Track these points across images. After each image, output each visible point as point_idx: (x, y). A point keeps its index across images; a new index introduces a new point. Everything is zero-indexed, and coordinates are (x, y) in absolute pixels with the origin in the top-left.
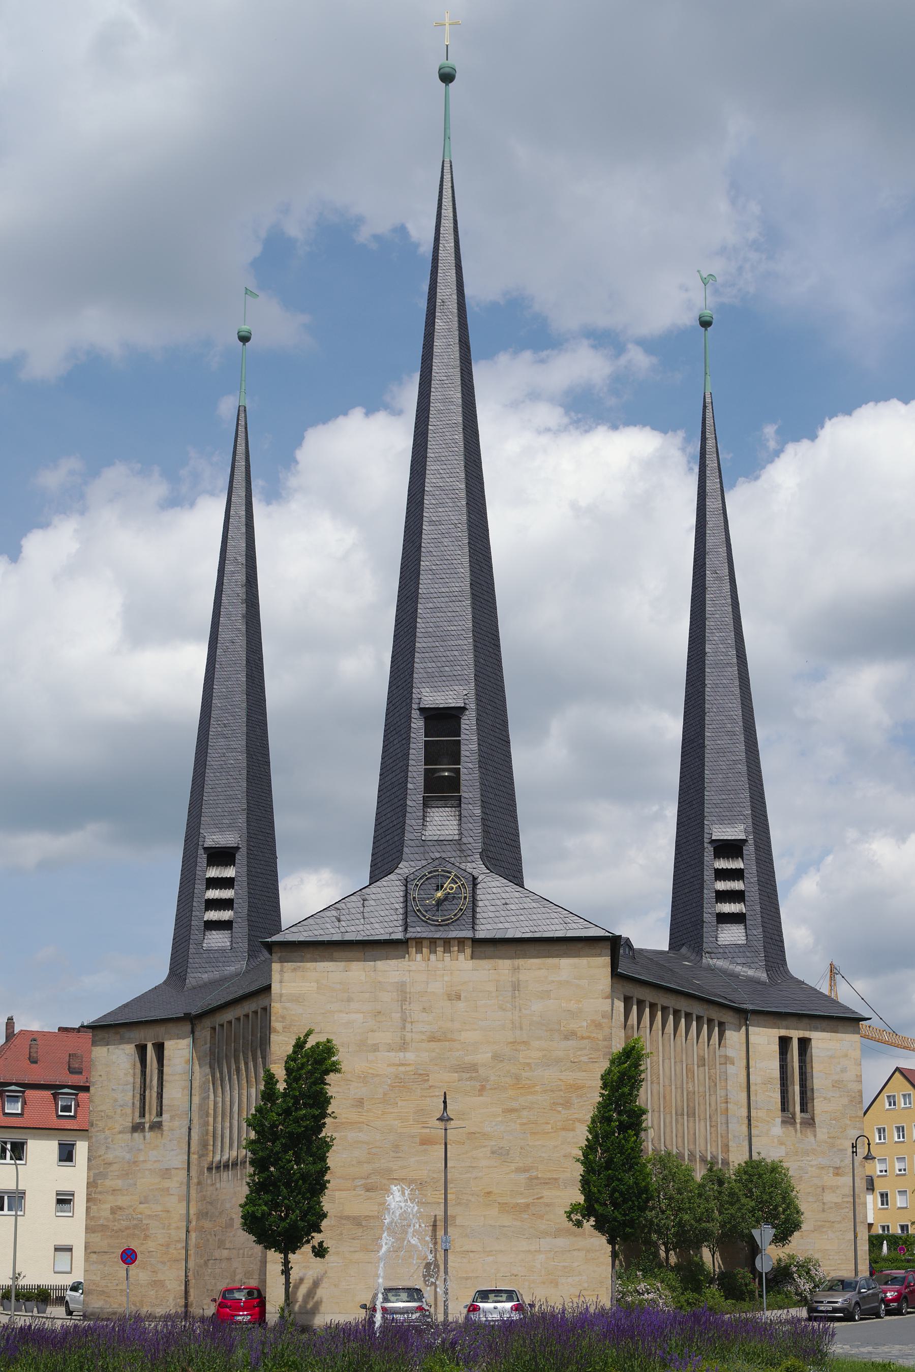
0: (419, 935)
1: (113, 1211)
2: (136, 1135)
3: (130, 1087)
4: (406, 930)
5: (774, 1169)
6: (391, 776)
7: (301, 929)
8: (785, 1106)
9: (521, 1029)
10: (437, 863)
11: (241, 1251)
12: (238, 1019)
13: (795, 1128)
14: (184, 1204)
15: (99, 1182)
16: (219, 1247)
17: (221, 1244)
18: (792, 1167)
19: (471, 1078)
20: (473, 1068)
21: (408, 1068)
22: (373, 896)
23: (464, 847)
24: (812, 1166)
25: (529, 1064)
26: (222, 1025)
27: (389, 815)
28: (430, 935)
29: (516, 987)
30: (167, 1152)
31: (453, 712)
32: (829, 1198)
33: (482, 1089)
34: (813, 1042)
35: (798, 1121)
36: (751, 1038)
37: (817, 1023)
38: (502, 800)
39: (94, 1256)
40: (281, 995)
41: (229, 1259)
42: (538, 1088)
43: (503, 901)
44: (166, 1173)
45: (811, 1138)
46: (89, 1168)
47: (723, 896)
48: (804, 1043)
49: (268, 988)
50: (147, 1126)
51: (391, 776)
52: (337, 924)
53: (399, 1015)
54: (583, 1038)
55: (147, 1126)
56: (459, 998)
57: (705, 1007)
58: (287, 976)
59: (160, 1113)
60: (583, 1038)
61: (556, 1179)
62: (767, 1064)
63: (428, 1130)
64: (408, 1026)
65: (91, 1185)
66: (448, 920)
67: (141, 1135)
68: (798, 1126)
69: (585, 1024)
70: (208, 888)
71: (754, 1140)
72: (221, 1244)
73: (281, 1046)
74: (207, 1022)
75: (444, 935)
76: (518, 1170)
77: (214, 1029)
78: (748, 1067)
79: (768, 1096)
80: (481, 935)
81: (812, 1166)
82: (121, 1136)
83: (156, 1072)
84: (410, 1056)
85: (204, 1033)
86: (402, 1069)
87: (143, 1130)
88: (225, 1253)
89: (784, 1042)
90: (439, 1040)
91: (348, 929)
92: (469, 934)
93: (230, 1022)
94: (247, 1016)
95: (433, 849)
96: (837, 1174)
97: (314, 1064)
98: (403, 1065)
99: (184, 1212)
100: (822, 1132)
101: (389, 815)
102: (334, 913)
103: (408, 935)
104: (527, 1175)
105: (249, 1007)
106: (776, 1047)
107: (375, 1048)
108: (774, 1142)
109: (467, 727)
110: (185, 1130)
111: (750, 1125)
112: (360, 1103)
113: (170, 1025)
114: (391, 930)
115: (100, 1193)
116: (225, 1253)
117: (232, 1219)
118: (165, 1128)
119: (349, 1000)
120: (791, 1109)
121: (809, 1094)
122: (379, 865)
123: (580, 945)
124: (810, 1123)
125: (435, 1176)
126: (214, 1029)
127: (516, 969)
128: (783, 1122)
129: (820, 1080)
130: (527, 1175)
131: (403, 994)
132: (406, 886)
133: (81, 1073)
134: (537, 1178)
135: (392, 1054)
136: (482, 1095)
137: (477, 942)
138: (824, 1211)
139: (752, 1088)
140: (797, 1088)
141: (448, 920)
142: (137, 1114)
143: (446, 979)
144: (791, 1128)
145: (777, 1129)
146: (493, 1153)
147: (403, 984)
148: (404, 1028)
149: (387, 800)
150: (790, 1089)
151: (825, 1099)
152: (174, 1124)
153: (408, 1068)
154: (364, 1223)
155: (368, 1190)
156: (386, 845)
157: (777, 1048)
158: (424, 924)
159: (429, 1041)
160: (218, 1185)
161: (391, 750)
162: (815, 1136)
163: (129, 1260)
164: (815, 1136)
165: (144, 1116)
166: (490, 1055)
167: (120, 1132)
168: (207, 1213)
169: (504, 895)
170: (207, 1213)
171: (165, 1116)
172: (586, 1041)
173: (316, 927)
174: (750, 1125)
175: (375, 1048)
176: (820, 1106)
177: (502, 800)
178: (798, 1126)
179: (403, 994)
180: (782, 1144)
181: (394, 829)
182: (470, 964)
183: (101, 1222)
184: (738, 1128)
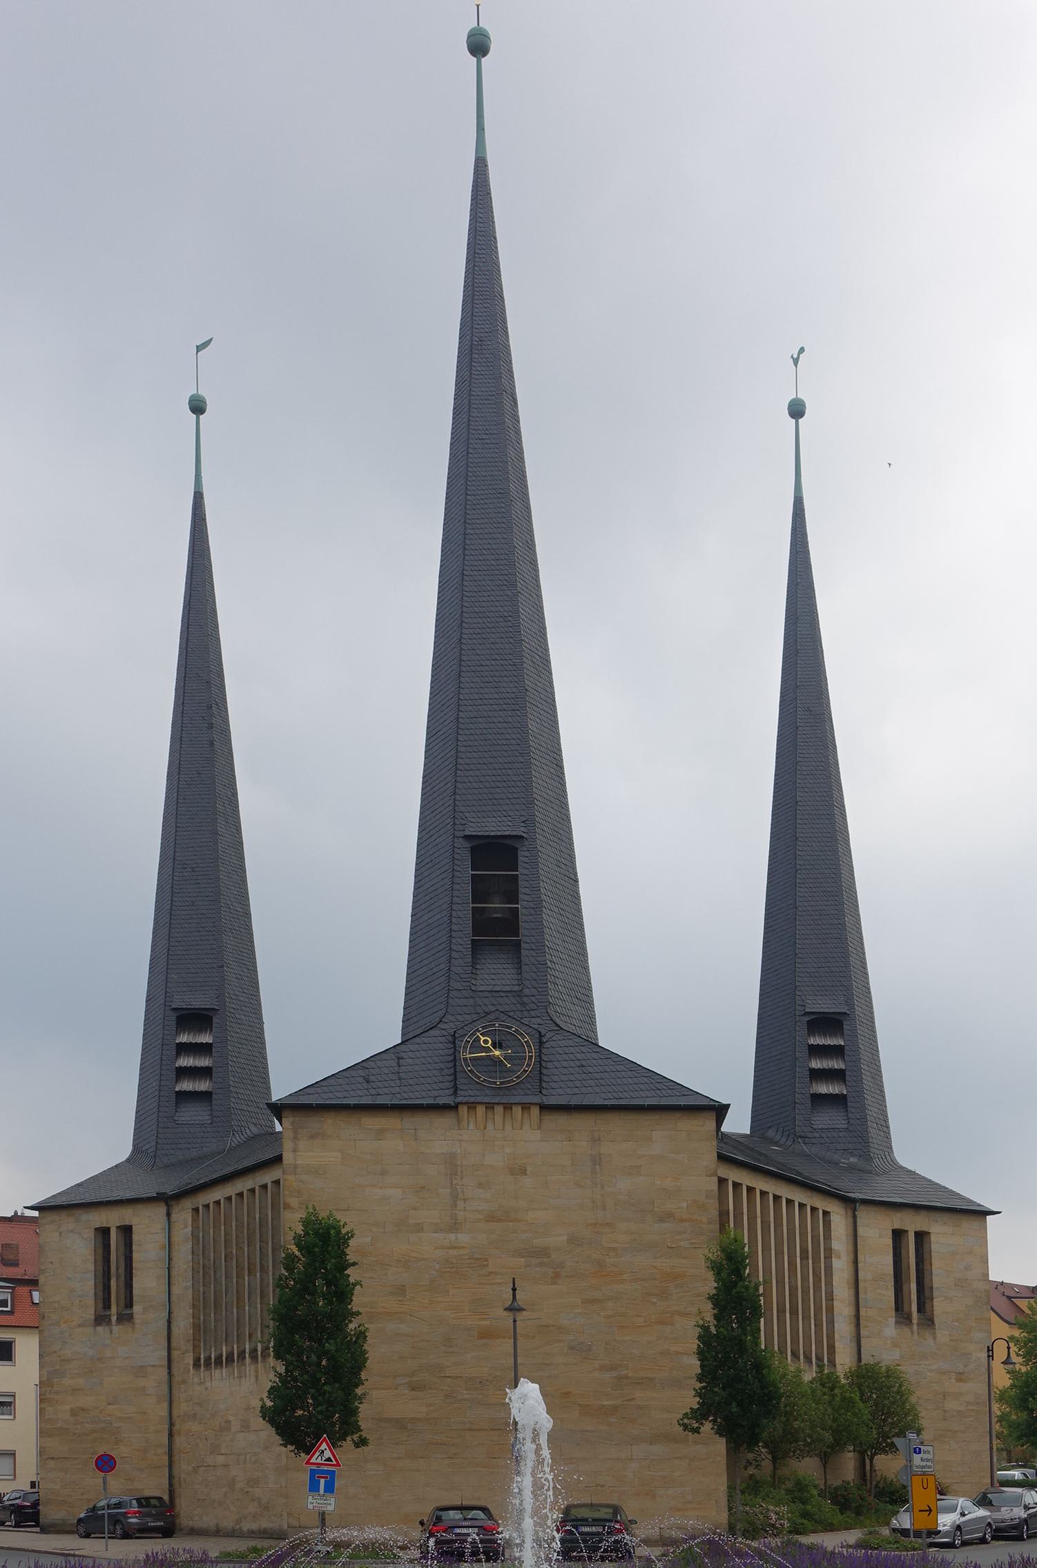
0: (472, 1100)
1: (74, 1413)
2: (100, 1329)
3: (91, 1276)
4: (455, 1093)
5: (890, 1373)
6: (426, 917)
7: (319, 1090)
8: (899, 1305)
9: (604, 1208)
10: (491, 1017)
11: (242, 1457)
12: (229, 1199)
13: (911, 1329)
14: (166, 1404)
15: (55, 1380)
16: (212, 1453)
17: (215, 1450)
18: (908, 1370)
19: (541, 1264)
20: (544, 1252)
21: (461, 1252)
22: (411, 1054)
23: (525, 1000)
24: (931, 1371)
25: (614, 1249)
26: (207, 1206)
27: (425, 962)
28: (486, 1100)
29: (597, 1160)
30: (138, 1346)
31: (508, 842)
32: (951, 1405)
33: (557, 1276)
34: (933, 1238)
35: (915, 1321)
36: (860, 1231)
37: (937, 1215)
38: (572, 947)
39: (52, 1463)
40: (295, 1167)
41: (226, 1466)
42: (625, 1276)
43: (578, 1063)
44: (141, 1371)
45: (931, 1341)
46: (41, 1367)
47: (817, 1075)
48: (921, 1236)
49: (278, 1159)
50: (114, 1318)
51: (426, 917)
52: (365, 1085)
53: (448, 1191)
54: (682, 1220)
55: (114, 1318)
56: (523, 1172)
57: (809, 1194)
58: (302, 1144)
59: (130, 1304)
60: (682, 1220)
61: (650, 1379)
62: (879, 1261)
63: (488, 1323)
64: (461, 1204)
65: (45, 1384)
66: (508, 1082)
67: (107, 1329)
68: (915, 1327)
69: (684, 1205)
70: (178, 1054)
71: (863, 1341)
72: (215, 1450)
73: (293, 1222)
74: (188, 1204)
75: (504, 1100)
76: (603, 1368)
77: (196, 1210)
78: (856, 1262)
79: (880, 1295)
80: (552, 1101)
81: (931, 1371)
82: (80, 1329)
83: (122, 1259)
84: (463, 1238)
85: (183, 1215)
86: (454, 1252)
87: (109, 1323)
88: (221, 1459)
89: (898, 1235)
90: (500, 1220)
91: (380, 1091)
92: (537, 1099)
93: (218, 1203)
94: (240, 1195)
95: (486, 1001)
96: (960, 1380)
97: (325, 1248)
98: (455, 1248)
99: (165, 1413)
100: (943, 1335)
101: (425, 962)
102: (361, 1072)
103: (459, 1099)
104: (615, 1374)
105: (267, 1177)
106: (888, 1241)
107: (419, 1228)
108: (887, 1343)
109: (526, 860)
110: (163, 1323)
111: (858, 1325)
112: (401, 1290)
113: (140, 1206)
114: (435, 1093)
115: (57, 1393)
116: (221, 1459)
117: (228, 1422)
118: (137, 1321)
119: (384, 1173)
120: (906, 1309)
121: (927, 1292)
122: (415, 1020)
123: (678, 1115)
124: (928, 1321)
125: (498, 1373)
126: (196, 1210)
127: (596, 1141)
128: (897, 1322)
129: (939, 1278)
130: (615, 1374)
131: (453, 1167)
132: (454, 1043)
133: (17, 1265)
134: (627, 1377)
135: (440, 1236)
136: (555, 1283)
137: (544, 1108)
138: (945, 1419)
139: (861, 1285)
140: (914, 1286)
141: (508, 1082)
142: (101, 1306)
143: (508, 1150)
144: (906, 1329)
145: (890, 1329)
146: (572, 1348)
147: (453, 1156)
148: (455, 1205)
149: (423, 944)
150: (905, 1287)
151: (946, 1298)
152: (147, 1314)
153: (461, 1252)
154: (409, 1426)
155: (413, 1390)
156: (422, 997)
157: (890, 1241)
158: (478, 1087)
159: (487, 1221)
160: (208, 1384)
161: (426, 886)
162: (935, 1339)
163: (106, 1467)
164: (935, 1339)
165: (109, 1308)
166: (565, 1238)
167: (80, 1326)
168: (195, 1415)
169: (578, 1056)
170: (195, 1415)
171: (137, 1308)
172: (686, 1224)
173: (338, 1088)
174: (858, 1325)
175: (419, 1228)
176: (939, 1306)
177: (572, 947)
178: (915, 1327)
179: (453, 1167)
180: (895, 1345)
181: (434, 977)
182: (537, 1135)
183: (59, 1425)
184: (843, 1328)
